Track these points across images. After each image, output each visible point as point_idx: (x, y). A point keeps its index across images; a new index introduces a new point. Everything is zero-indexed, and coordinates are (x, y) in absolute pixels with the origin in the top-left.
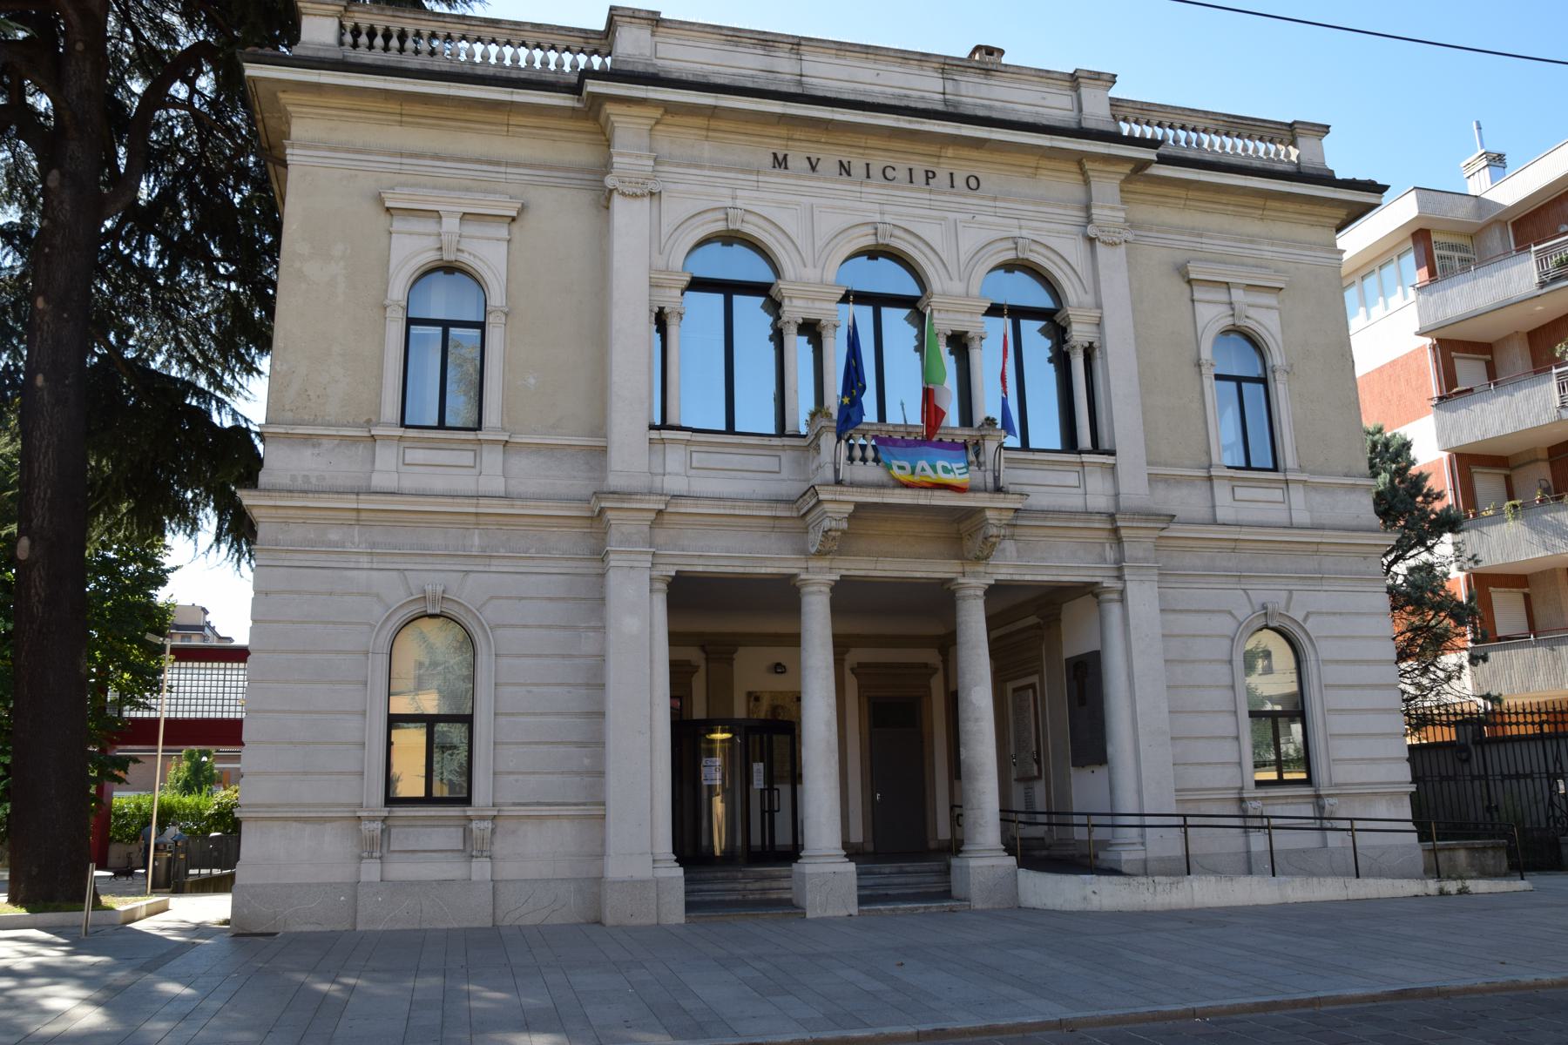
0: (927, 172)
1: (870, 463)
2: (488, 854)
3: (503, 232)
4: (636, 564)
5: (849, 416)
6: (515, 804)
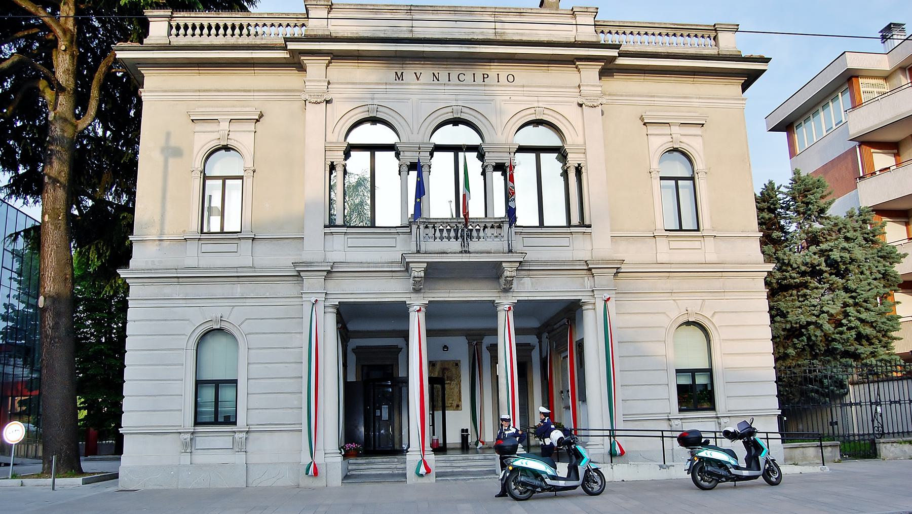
0: (484, 74)
1: (452, 239)
2: (244, 450)
3: (251, 126)
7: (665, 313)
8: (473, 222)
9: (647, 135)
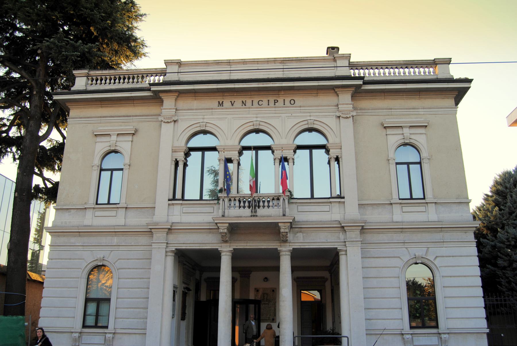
0: (275, 100)
3: (130, 138)
4: (160, 247)
5: (228, 190)
6: (121, 329)
7: (399, 257)
8: (260, 196)
9: (387, 135)
